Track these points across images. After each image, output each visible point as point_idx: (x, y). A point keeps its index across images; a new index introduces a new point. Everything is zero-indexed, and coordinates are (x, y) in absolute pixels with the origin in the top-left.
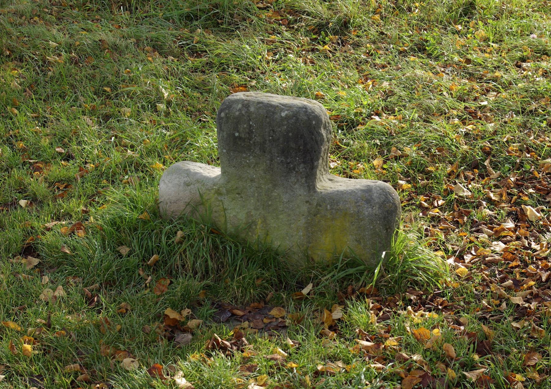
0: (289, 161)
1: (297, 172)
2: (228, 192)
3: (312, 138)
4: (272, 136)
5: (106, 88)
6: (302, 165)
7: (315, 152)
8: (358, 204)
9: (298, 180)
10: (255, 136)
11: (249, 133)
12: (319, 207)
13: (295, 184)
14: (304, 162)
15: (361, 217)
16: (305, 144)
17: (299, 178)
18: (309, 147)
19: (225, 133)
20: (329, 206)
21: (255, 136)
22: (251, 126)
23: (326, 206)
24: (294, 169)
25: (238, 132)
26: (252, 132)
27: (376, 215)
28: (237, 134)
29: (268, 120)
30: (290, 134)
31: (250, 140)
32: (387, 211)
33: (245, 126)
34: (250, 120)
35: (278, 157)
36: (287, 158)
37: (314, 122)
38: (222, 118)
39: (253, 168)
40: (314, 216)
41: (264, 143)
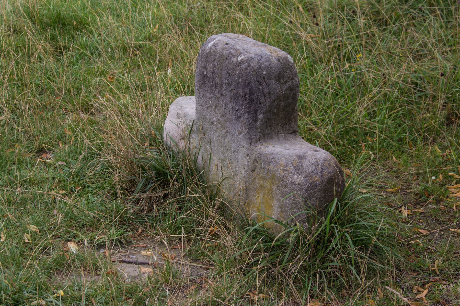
8: (286, 169)
14: (248, 112)
18: (254, 97)
27: (299, 184)
30: (240, 80)
35: (231, 102)
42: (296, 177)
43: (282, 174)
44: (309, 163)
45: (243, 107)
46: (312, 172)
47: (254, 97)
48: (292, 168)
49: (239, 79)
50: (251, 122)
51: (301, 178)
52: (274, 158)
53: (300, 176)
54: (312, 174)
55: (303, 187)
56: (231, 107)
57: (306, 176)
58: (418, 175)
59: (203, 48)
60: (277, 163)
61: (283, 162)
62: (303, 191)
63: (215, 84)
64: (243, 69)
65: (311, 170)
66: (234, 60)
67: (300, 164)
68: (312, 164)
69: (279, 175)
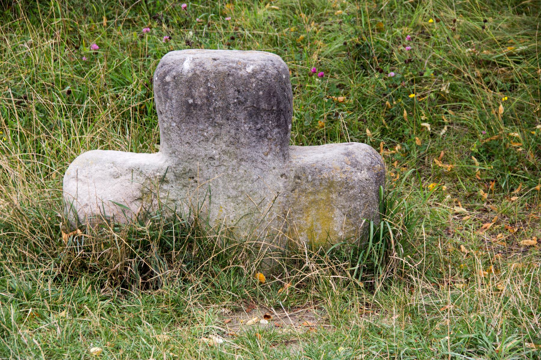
0: (259, 126)
1: (270, 139)
2: (177, 177)
3: (285, 96)
4: (237, 98)
5: (405, 112)
6: (276, 130)
7: (288, 112)
8: (343, 170)
9: (271, 149)
10: (215, 100)
11: (207, 98)
12: (297, 180)
13: (267, 155)
14: (278, 126)
15: (351, 184)
16: (279, 103)
17: (273, 146)
18: (282, 106)
19: (174, 101)
20: (310, 177)
21: (215, 100)
22: (209, 88)
23: (307, 177)
24: (266, 135)
25: (192, 97)
26: (212, 96)
27: (366, 180)
28: (191, 101)
29: (231, 78)
30: (261, 93)
31: (210, 106)
32: (377, 174)
33: (201, 89)
34: (207, 80)
35: (245, 123)
36: (257, 123)
37: (284, 77)
38: (168, 83)
39: (212, 142)
40: (292, 191)
41: (228, 107)
42: (359, 174)
43: (344, 176)
44: (362, 157)
45: (270, 122)
46: (372, 163)
47: (282, 106)
48: (349, 167)
49: (257, 92)
50: (282, 135)
51: (364, 173)
52: (323, 165)
53: (363, 172)
54: (373, 164)
55: (372, 180)
56: (247, 129)
57: (369, 169)
58: (43, 188)
59: (499, 43)
60: (330, 168)
61: (337, 165)
62: (374, 184)
63: (214, 108)
64: (261, 80)
65: (369, 162)
66: (242, 72)
67: (354, 161)
68: (365, 156)
69: (340, 179)
